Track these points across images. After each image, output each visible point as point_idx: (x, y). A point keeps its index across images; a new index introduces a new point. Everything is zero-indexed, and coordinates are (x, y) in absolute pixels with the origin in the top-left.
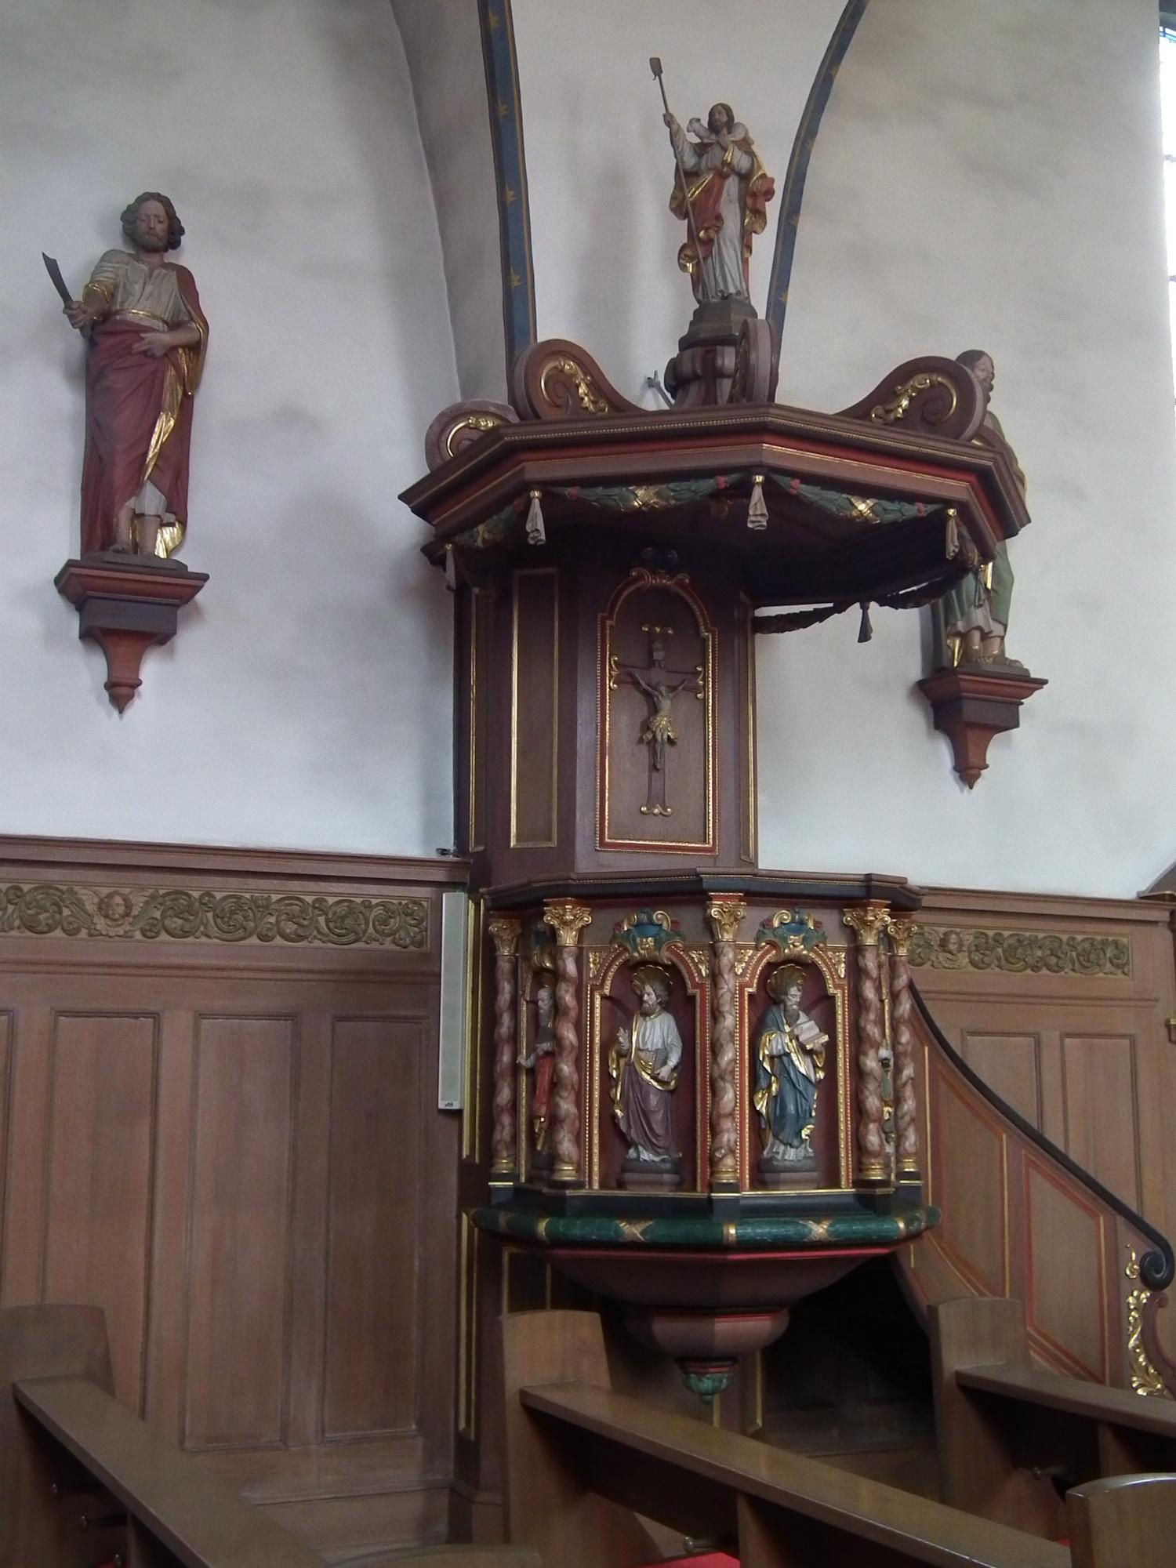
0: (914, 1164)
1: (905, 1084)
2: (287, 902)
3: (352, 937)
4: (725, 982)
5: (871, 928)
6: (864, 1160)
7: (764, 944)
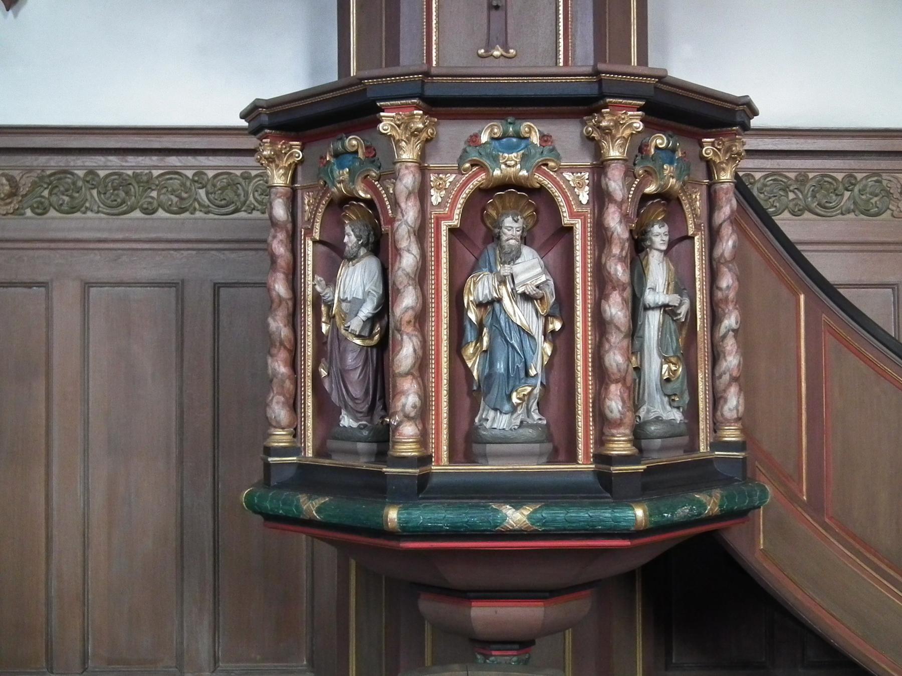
0: (738, 433)
1: (724, 337)
2: (168, 176)
3: (232, 208)
4: (402, 212)
5: (613, 138)
6: (606, 431)
7: (467, 165)
